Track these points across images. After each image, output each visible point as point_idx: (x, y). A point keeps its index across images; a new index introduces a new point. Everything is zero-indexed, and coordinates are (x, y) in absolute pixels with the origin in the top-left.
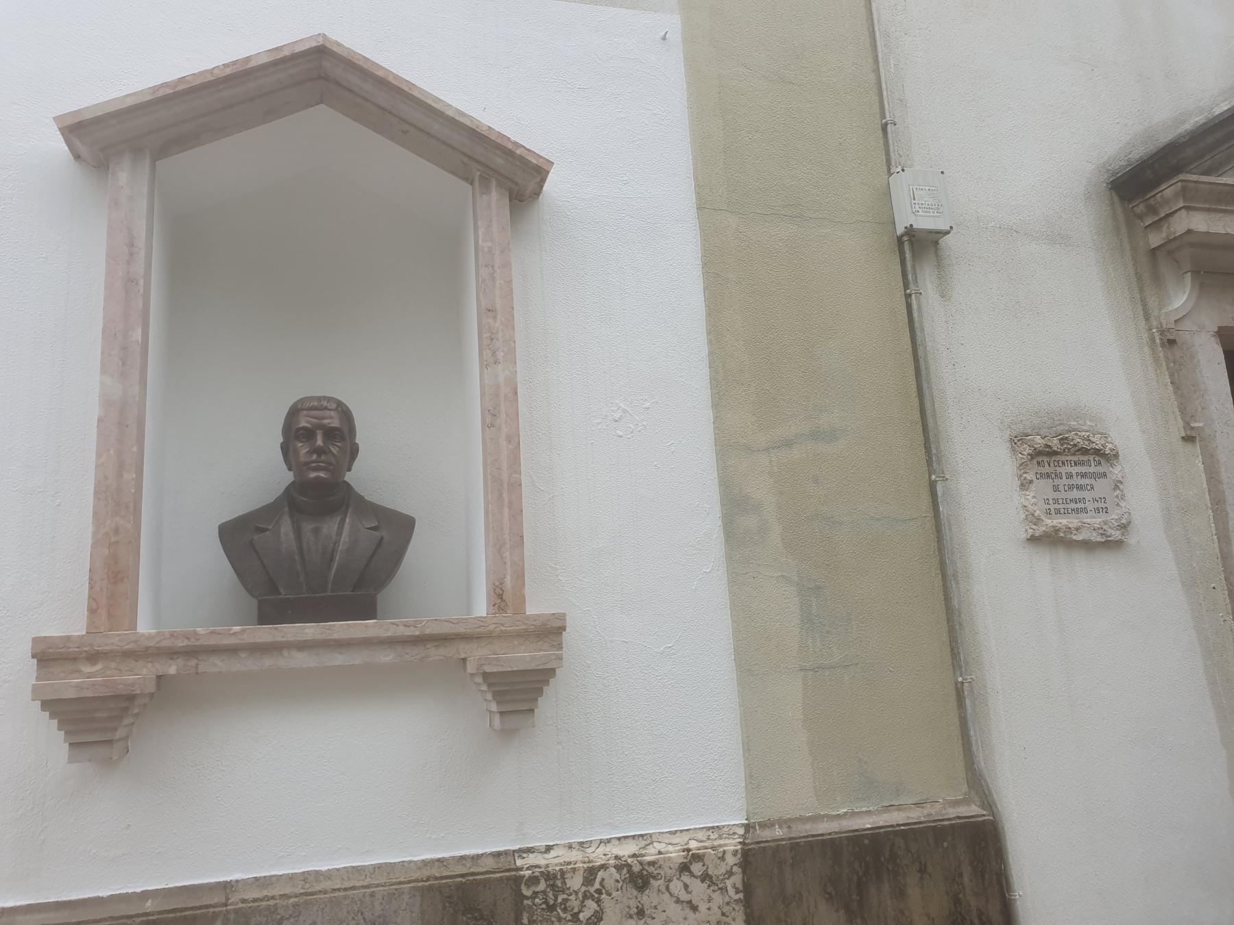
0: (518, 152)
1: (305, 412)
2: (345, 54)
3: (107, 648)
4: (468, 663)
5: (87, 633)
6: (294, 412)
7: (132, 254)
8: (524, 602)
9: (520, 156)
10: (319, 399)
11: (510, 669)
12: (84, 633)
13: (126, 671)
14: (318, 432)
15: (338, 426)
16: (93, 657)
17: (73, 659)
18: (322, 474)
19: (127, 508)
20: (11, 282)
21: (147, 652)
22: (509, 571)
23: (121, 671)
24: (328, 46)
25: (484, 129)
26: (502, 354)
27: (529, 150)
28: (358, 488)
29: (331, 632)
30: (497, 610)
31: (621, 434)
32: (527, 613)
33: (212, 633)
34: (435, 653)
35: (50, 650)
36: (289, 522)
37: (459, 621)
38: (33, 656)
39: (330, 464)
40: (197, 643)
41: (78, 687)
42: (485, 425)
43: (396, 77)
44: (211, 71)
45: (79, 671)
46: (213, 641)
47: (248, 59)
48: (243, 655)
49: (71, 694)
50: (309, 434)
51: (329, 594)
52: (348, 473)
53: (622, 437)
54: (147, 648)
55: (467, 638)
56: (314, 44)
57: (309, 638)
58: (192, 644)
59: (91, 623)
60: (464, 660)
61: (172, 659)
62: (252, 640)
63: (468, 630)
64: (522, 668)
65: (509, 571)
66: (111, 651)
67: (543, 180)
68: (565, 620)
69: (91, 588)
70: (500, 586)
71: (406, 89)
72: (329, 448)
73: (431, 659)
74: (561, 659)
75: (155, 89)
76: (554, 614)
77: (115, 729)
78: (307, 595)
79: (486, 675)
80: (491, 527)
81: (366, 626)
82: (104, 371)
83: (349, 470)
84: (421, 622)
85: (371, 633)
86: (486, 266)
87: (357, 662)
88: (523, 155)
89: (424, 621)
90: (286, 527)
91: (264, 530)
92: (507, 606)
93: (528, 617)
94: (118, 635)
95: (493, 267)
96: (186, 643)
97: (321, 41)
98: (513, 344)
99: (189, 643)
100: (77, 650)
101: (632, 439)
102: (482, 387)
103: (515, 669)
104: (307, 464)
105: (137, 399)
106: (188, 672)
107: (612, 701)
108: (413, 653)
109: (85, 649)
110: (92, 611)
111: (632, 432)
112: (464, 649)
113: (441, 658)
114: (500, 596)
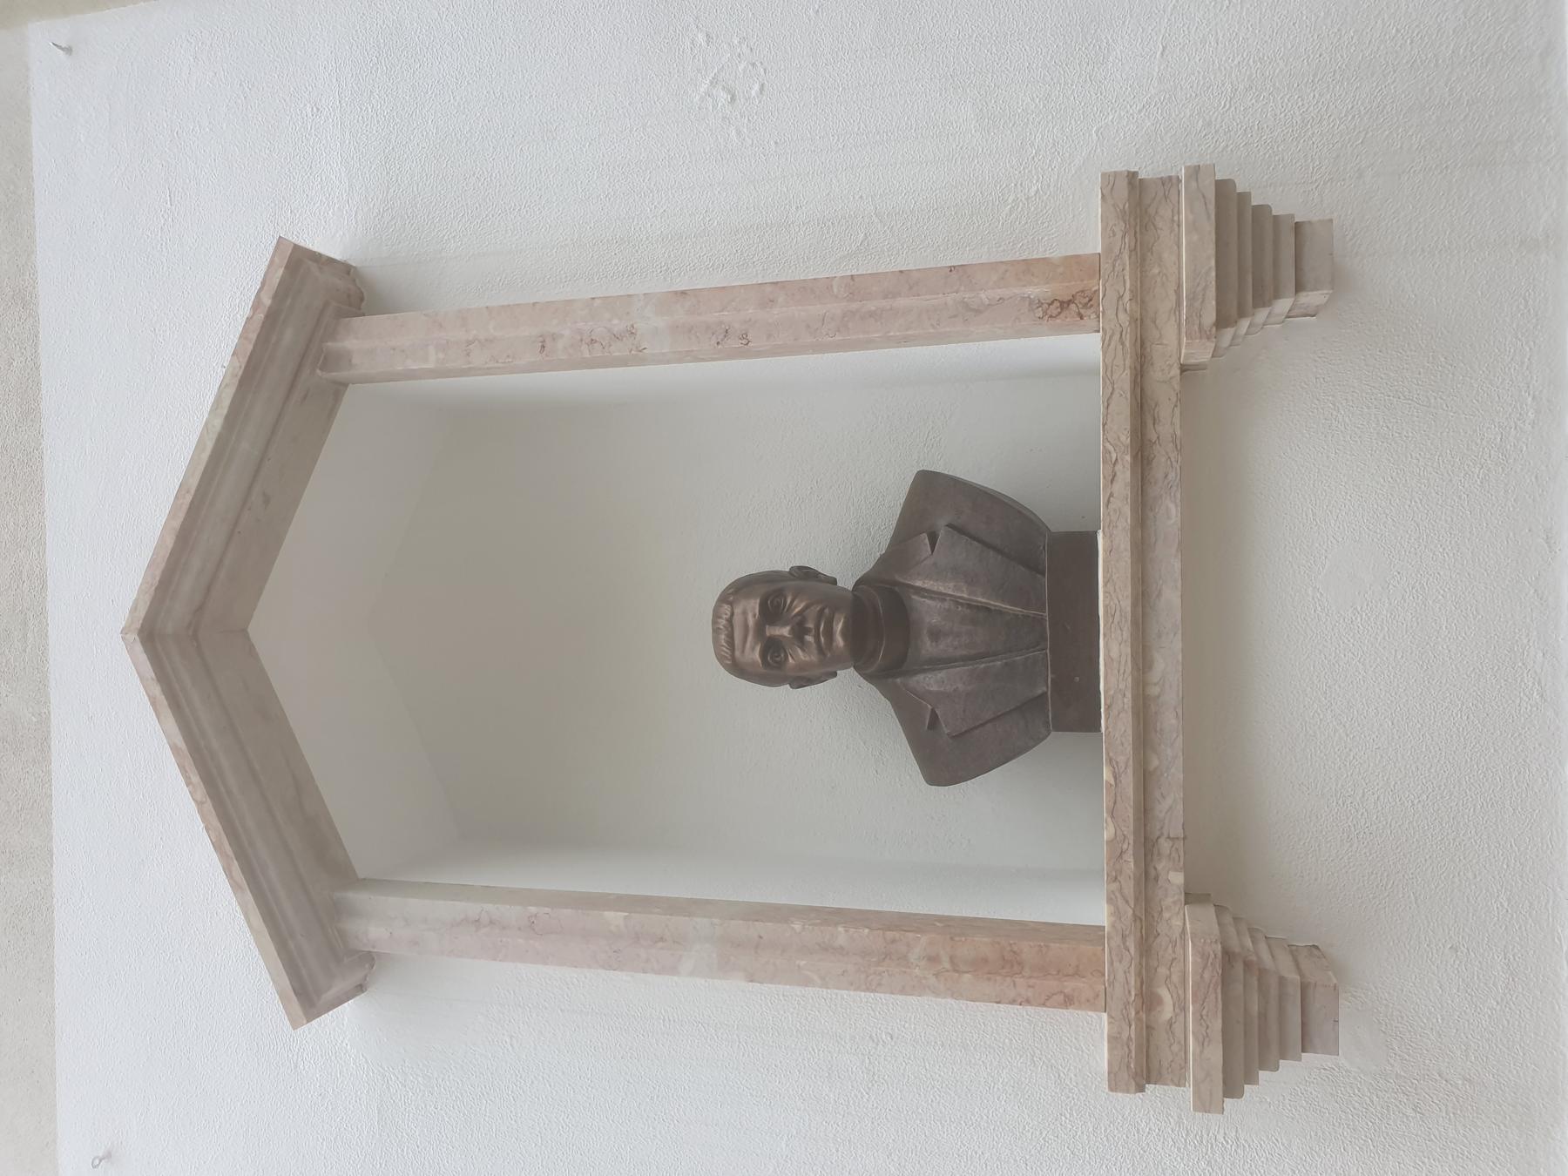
0: (267, 301)
1: (737, 653)
2: (148, 599)
3: (1133, 983)
4: (1192, 361)
5: (1105, 1011)
6: (738, 669)
7: (491, 922)
8: (1077, 259)
9: (275, 297)
10: (716, 631)
11: (1213, 274)
12: (1105, 1016)
13: (1174, 952)
14: (768, 634)
15: (758, 601)
16: (1148, 1000)
17: (1148, 1032)
18: (839, 627)
19: (893, 941)
20: (550, 1086)
21: (1143, 917)
22: (1017, 291)
23: (1174, 959)
24: (139, 626)
25: (238, 365)
26: (616, 321)
27: (263, 284)
28: (866, 565)
29: (1118, 613)
30: (1089, 312)
31: (757, 87)
32: (1099, 250)
33: (1112, 814)
34: (1168, 423)
35: (1132, 1066)
36: (920, 677)
37: (1109, 380)
38: (1141, 1089)
39: (821, 612)
40: (1131, 839)
41: (1202, 1042)
42: (745, 348)
43: (172, 514)
44: (200, 804)
45: (1170, 1023)
46: (1128, 811)
47: (175, 749)
48: (1154, 762)
49: (1215, 1054)
50: (772, 649)
51: (1047, 614)
52: (839, 584)
53: (763, 85)
54: (1136, 917)
55: (1142, 366)
56: (139, 648)
57: (1129, 650)
58: (1131, 847)
59: (1090, 1004)
60: (1184, 369)
61: (1156, 879)
62: (1129, 749)
63: (1128, 362)
64: (1211, 250)
65: (1017, 291)
66: (1139, 974)
67: (316, 257)
68: (1115, 172)
69: (1028, 1002)
70: (1046, 306)
71: (189, 498)
72: (796, 615)
73: (1178, 432)
74: (1197, 169)
75: (235, 887)
76: (1103, 196)
77: (1282, 981)
78: (1048, 651)
79: (1222, 322)
80: (932, 331)
81: (1109, 551)
82: (673, 970)
83: (834, 581)
84: (1107, 451)
85: (1124, 542)
86: (468, 355)
87: (1177, 565)
88: (272, 293)
89: (1104, 447)
90: (930, 681)
91: (934, 716)
92: (1082, 291)
93: (1108, 248)
94: (1111, 963)
95: (469, 343)
96: (1129, 857)
97: (133, 637)
98: (598, 302)
99: (1131, 852)
100: (1133, 1027)
101: (766, 64)
102: (681, 358)
103: (1213, 263)
104: (821, 650)
105: (716, 921)
106: (1182, 853)
107: (1281, 71)
108: (1165, 463)
109: (1133, 1013)
110: (1068, 1001)
111: (753, 65)
112: (1163, 373)
113: (1177, 411)
114: (1064, 305)
